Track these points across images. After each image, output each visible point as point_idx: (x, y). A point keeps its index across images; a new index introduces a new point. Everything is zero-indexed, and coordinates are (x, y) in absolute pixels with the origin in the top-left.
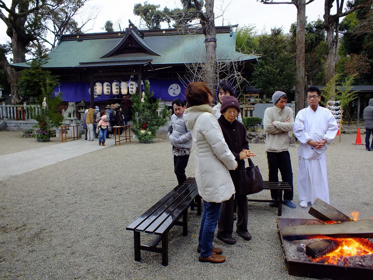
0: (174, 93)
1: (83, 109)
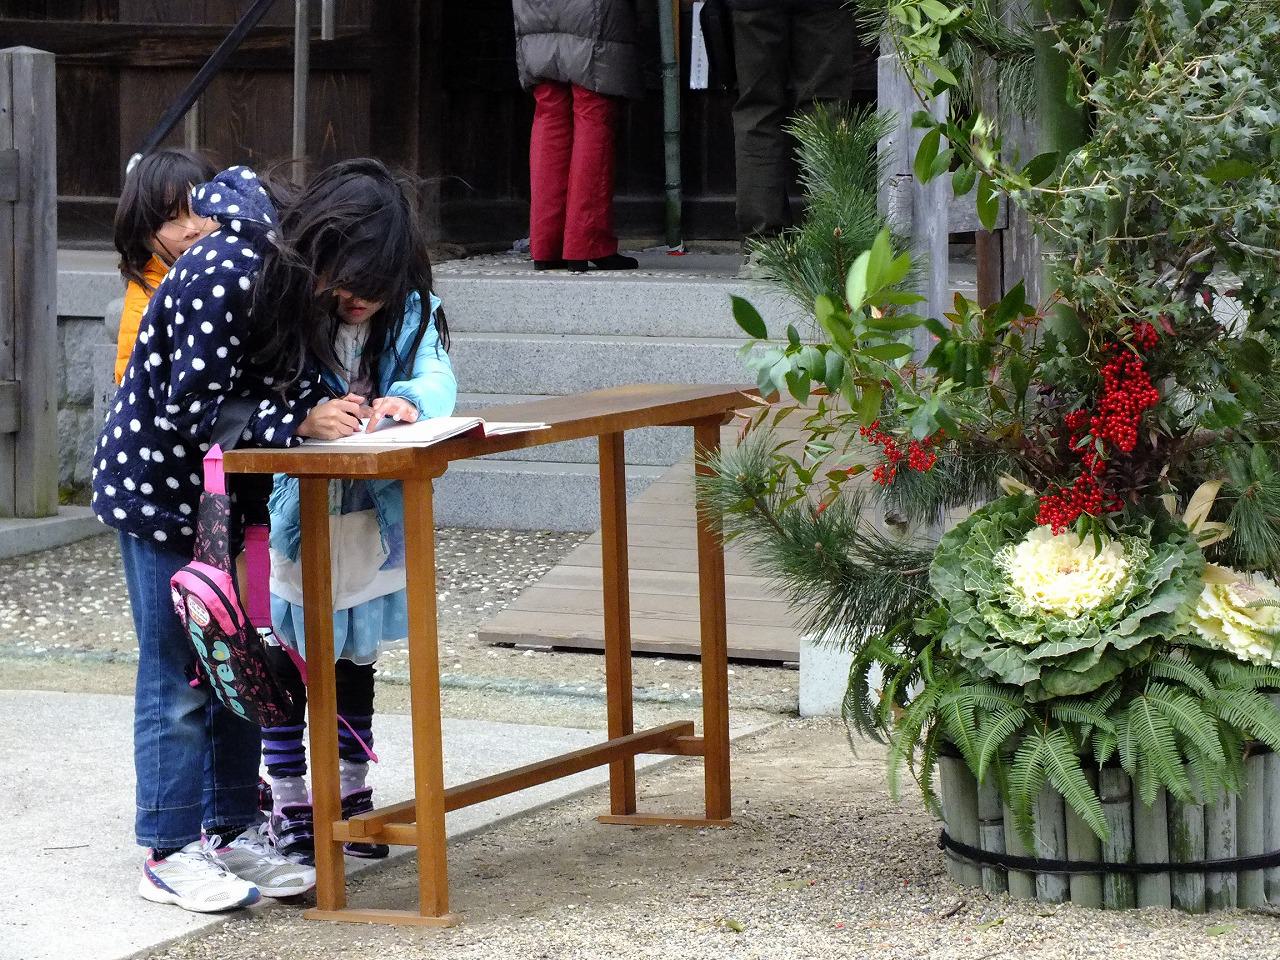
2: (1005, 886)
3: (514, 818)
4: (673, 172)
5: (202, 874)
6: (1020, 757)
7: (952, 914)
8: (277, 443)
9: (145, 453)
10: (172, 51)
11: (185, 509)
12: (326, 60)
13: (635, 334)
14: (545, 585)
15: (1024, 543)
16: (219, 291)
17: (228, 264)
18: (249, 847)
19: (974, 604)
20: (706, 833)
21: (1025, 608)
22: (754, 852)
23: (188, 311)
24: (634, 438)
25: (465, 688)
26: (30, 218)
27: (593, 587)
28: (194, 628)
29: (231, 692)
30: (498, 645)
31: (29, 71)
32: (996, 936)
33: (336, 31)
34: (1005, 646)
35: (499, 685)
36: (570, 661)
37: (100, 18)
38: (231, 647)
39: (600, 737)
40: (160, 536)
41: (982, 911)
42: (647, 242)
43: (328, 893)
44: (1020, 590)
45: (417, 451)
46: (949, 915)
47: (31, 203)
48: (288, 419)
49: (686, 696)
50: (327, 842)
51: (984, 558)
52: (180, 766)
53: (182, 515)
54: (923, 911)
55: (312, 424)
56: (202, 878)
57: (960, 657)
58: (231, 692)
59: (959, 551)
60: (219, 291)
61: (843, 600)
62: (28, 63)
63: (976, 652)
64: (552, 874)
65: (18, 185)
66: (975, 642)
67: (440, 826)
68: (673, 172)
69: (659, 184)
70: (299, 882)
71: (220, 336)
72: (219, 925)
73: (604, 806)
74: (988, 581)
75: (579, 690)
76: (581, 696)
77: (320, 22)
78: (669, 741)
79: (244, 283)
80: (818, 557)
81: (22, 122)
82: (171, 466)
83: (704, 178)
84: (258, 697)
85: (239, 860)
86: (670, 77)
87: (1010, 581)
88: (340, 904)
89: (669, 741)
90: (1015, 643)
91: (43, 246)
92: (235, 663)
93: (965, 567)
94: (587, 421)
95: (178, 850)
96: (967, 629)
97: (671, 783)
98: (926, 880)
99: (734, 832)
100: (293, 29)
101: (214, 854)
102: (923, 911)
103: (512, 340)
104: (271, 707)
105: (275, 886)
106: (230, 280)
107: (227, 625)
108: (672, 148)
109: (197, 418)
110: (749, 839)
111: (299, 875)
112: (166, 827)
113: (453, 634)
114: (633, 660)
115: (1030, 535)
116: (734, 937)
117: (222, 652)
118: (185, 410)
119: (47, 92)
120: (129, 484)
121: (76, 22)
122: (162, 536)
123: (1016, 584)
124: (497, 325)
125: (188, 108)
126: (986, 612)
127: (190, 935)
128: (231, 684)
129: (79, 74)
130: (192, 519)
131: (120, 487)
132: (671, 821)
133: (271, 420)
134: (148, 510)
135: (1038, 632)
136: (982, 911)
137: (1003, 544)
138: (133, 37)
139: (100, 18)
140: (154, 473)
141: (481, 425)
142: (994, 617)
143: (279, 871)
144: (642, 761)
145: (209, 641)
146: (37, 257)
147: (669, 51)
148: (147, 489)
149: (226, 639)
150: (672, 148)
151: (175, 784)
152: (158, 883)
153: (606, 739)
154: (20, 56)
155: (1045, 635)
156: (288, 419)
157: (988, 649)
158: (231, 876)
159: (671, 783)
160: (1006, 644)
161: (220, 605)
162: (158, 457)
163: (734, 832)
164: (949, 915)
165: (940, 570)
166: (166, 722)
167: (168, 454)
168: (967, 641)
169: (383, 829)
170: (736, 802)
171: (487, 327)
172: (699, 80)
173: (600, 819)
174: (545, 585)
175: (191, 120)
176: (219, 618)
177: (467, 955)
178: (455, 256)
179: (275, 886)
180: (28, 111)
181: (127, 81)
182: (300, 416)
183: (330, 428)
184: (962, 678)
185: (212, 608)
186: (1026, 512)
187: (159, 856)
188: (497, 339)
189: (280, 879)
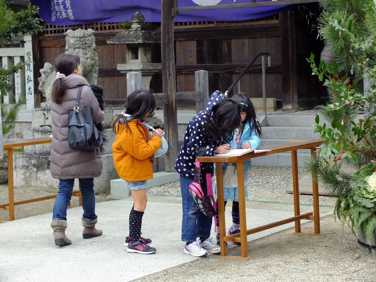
2: (371, 252)
3: (275, 233)
5: (196, 248)
6: (370, 222)
7: (357, 258)
8: (209, 155)
9: (185, 157)
11: (193, 170)
12: (269, 71)
14: (301, 181)
15: (372, 175)
16: (197, 125)
17: (200, 119)
18: (208, 242)
19: (360, 189)
20: (314, 237)
21: (371, 190)
22: (322, 242)
23: (192, 128)
24: (298, 151)
25: (280, 203)
26: (203, 105)
27: (310, 181)
28: (194, 197)
29: (203, 210)
30: (290, 193)
31: (202, 75)
32: (364, 265)
33: (271, 65)
34: (367, 199)
35: (287, 202)
36: (303, 197)
37: (229, 63)
38: (201, 201)
39: (292, 215)
40: (187, 175)
41: (364, 258)
43: (223, 253)
44: (370, 186)
45: (238, 157)
46: (356, 259)
48: (212, 149)
49: (324, 204)
50: (223, 241)
51: (362, 179)
52: (190, 225)
53: (192, 171)
54: (351, 258)
55: (217, 150)
56: (196, 249)
57: (356, 201)
58: (203, 210)
59: (357, 177)
60: (197, 125)
61: (336, 188)
62: (202, 73)
63: (360, 201)
64: (277, 248)
65: (201, 99)
66: (359, 198)
67: (246, 238)
70: (218, 250)
71: (198, 134)
72: (198, 259)
73: (294, 231)
74: (363, 184)
75: (303, 203)
76: (303, 204)
77: (268, 63)
78: (307, 217)
79: (202, 123)
80: (330, 177)
81: (201, 85)
82: (190, 160)
84: (208, 211)
85: (205, 245)
87: (368, 184)
88: (225, 255)
89: (307, 217)
90: (368, 198)
92: (202, 204)
93: (358, 181)
94: (282, 149)
95: (191, 243)
96: (358, 195)
97: (307, 225)
98: (354, 250)
99: (320, 237)
100: (262, 64)
101: (199, 244)
102: (351, 258)
103: (306, 128)
104: (211, 213)
105: (213, 251)
106: (199, 122)
107: (200, 196)
109: (193, 151)
110: (322, 238)
111: (218, 249)
112: (189, 237)
113: (281, 191)
114: (319, 196)
115: (373, 173)
116: (307, 263)
117: (200, 202)
118: (190, 149)
119: (206, 80)
120: (181, 164)
121: (224, 64)
122: (187, 177)
123: (369, 185)
125: (238, 81)
126: (362, 191)
127: (191, 262)
128: (202, 208)
129: (225, 74)
130: (194, 172)
131: (180, 164)
132: (307, 234)
133: (209, 150)
134: (185, 170)
135: (374, 195)
136: (364, 258)
137: (367, 175)
138: (234, 67)
139: (229, 63)
140: (186, 162)
141: (254, 151)
142: (364, 192)
143: (214, 247)
144: (302, 221)
145: (197, 200)
148: (185, 165)
149: (200, 199)
151: (190, 228)
152: (187, 250)
153: (294, 216)
155: (375, 196)
156: (212, 149)
157: (362, 200)
158: (202, 249)
159: (307, 225)
160: (366, 198)
161: (198, 191)
162: (187, 158)
163: (320, 237)
164: (356, 259)
165: (352, 182)
166: (187, 215)
167: (189, 158)
168: (358, 198)
169: (234, 239)
170: (321, 229)
171: (302, 125)
173: (293, 234)
174: (301, 181)
176: (198, 195)
177: (190, 280)
178: (300, 110)
179: (213, 251)
182: (214, 149)
183: (221, 152)
184: (357, 206)
185: (196, 192)
186: (373, 168)
187: (188, 244)
188: (303, 128)
189: (214, 249)
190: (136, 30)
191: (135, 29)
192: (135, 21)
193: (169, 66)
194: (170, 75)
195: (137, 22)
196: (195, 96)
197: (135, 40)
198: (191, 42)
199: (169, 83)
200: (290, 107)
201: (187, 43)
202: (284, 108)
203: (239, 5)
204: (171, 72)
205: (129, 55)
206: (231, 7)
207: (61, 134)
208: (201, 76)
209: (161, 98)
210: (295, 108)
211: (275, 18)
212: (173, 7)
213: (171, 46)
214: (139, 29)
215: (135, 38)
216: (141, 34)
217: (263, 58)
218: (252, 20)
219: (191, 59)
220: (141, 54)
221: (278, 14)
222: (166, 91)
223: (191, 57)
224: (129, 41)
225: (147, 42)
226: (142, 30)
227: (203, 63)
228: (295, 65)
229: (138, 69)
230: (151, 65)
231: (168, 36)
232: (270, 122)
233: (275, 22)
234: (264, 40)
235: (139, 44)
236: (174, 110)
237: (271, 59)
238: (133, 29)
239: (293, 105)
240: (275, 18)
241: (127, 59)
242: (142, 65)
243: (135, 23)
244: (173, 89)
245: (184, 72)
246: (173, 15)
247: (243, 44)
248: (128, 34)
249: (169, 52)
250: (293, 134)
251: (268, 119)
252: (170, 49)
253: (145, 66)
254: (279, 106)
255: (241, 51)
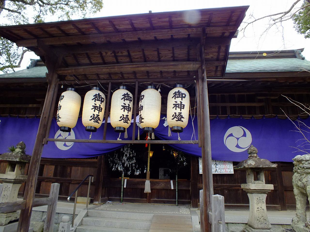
0: (238, 146)
1: (14, 171)
4: (122, 196)
10: (76, 182)
13: (125, 219)
26: (53, 207)
42: (119, 202)
47: (53, 205)
68: (122, 196)
69: (120, 196)
81: (54, 194)
83: (124, 196)
86: (122, 186)
91: (54, 211)
108: (122, 193)
124: (109, 217)
125: (76, 191)
138: (71, 180)
146: (53, 213)
147: (122, 184)
150: (122, 193)
154: (55, 185)
172: (125, 187)
175: (77, 192)
180: (55, 192)
181: (71, 185)
190: (18, 153)
191: (17, 152)
192: (18, 147)
193: (32, 180)
194: (31, 186)
195: (20, 148)
196: (48, 201)
197: (14, 158)
198: (52, 166)
199: (29, 192)
200: (97, 203)
201: (50, 166)
202: (94, 203)
203: (93, 141)
204: (33, 184)
205: (8, 169)
206: (87, 142)
207: (10, 190)
208: (55, 187)
209: (19, 205)
210: (99, 204)
211: (95, 158)
212: (45, 137)
213: (37, 165)
214: (20, 152)
215: (15, 157)
216: (20, 155)
217: (90, 177)
218: (86, 158)
219: (50, 174)
220: (17, 169)
221: (98, 157)
222: (26, 198)
223: (51, 173)
224: (10, 159)
225: (22, 161)
226: (22, 153)
227: (56, 177)
228: (102, 182)
229: (12, 179)
230: (22, 177)
231: (37, 157)
232: (89, 214)
233: (95, 160)
234: (89, 168)
235: (17, 162)
236: (29, 214)
237: (94, 178)
238: (16, 152)
239: (98, 202)
240: (95, 158)
241: (7, 171)
242: (15, 176)
243: (18, 148)
244: (32, 197)
245: (46, 181)
246: (43, 143)
247: (78, 170)
248: (11, 154)
249: (35, 169)
250: (103, 223)
251: (88, 212)
252: (36, 167)
253: (18, 177)
254: (92, 202)
255: (76, 173)
